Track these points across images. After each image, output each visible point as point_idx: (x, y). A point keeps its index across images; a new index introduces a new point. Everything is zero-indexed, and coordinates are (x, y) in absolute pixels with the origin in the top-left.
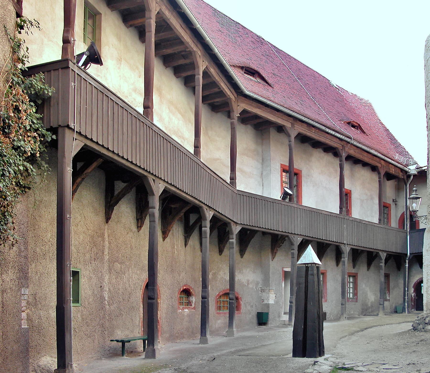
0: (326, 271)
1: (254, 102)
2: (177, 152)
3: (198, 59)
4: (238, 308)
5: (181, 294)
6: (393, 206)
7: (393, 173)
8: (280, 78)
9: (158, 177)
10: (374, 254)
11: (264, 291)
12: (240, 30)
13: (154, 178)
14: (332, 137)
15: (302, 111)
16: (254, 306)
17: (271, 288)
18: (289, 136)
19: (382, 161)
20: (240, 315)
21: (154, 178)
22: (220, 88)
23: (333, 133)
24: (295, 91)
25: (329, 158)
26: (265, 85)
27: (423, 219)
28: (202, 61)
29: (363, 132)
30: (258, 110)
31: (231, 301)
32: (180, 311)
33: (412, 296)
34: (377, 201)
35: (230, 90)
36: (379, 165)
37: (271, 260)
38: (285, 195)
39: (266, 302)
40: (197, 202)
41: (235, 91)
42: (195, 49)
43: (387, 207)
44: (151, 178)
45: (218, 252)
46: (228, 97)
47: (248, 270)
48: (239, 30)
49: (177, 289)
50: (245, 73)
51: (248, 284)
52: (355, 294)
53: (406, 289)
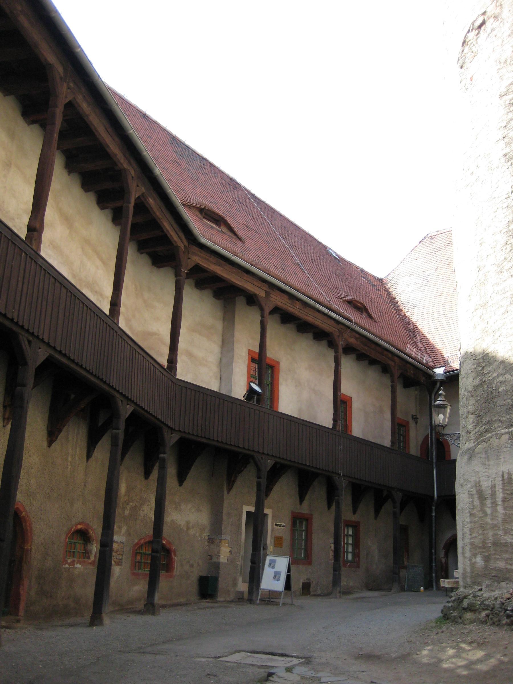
0: (311, 515)
1: (213, 257)
2: (102, 324)
3: (130, 180)
4: (169, 567)
5: (71, 537)
6: (412, 425)
7: (412, 376)
8: (256, 232)
9: (37, 337)
10: (385, 494)
11: (212, 543)
12: (207, 167)
13: (31, 338)
14: (326, 317)
15: (283, 277)
16: (195, 565)
17: (223, 537)
18: (262, 309)
19: (396, 358)
20: (171, 579)
21: (31, 338)
22: (163, 231)
23: (326, 311)
24: (276, 252)
25: (322, 347)
26: (232, 237)
27: (455, 438)
28: (135, 185)
29: (370, 317)
30: (218, 267)
31: (157, 556)
32: (67, 566)
33: (441, 562)
34: (388, 415)
35: (178, 234)
36: (391, 363)
37: (225, 492)
38: (251, 391)
39: (215, 560)
40: (105, 387)
41: (186, 237)
42: (126, 166)
43: (405, 426)
44: (24, 338)
45: (143, 474)
46: (175, 244)
47: (190, 506)
48: (204, 166)
49: (65, 529)
50: (204, 218)
51: (188, 528)
52: (355, 555)
53: (433, 551)
